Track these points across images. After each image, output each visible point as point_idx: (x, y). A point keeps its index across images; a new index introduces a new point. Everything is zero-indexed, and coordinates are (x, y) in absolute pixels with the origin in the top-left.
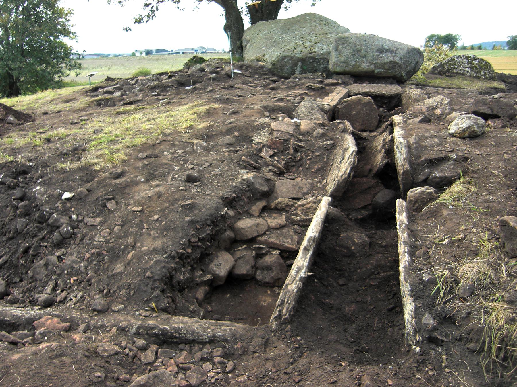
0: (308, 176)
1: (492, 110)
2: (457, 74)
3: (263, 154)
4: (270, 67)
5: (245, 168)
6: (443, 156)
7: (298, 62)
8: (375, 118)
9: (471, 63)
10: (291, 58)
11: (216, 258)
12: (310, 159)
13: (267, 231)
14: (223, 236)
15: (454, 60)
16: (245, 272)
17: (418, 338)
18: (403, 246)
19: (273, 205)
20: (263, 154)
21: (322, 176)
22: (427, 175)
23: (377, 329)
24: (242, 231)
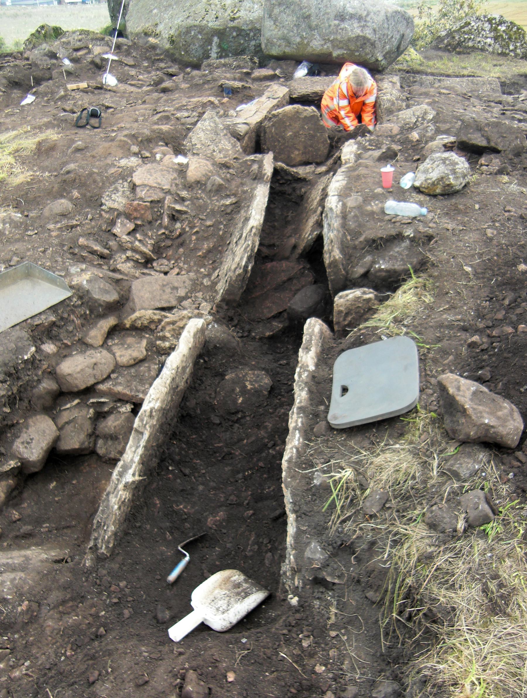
0: (192, 264)
1: (488, 140)
2: (474, 49)
3: (117, 230)
4: (168, 46)
5: (83, 260)
6: (394, 234)
7: (213, 36)
8: (323, 142)
9: (496, 30)
10: (201, 29)
11: (25, 430)
12: (197, 232)
13: (113, 372)
14: (36, 391)
15: (470, 24)
16: (77, 446)
17: (296, 583)
18: (295, 416)
19: (128, 323)
20: (117, 230)
21: (214, 262)
22: (368, 265)
23: (251, 553)
24: (69, 379)
